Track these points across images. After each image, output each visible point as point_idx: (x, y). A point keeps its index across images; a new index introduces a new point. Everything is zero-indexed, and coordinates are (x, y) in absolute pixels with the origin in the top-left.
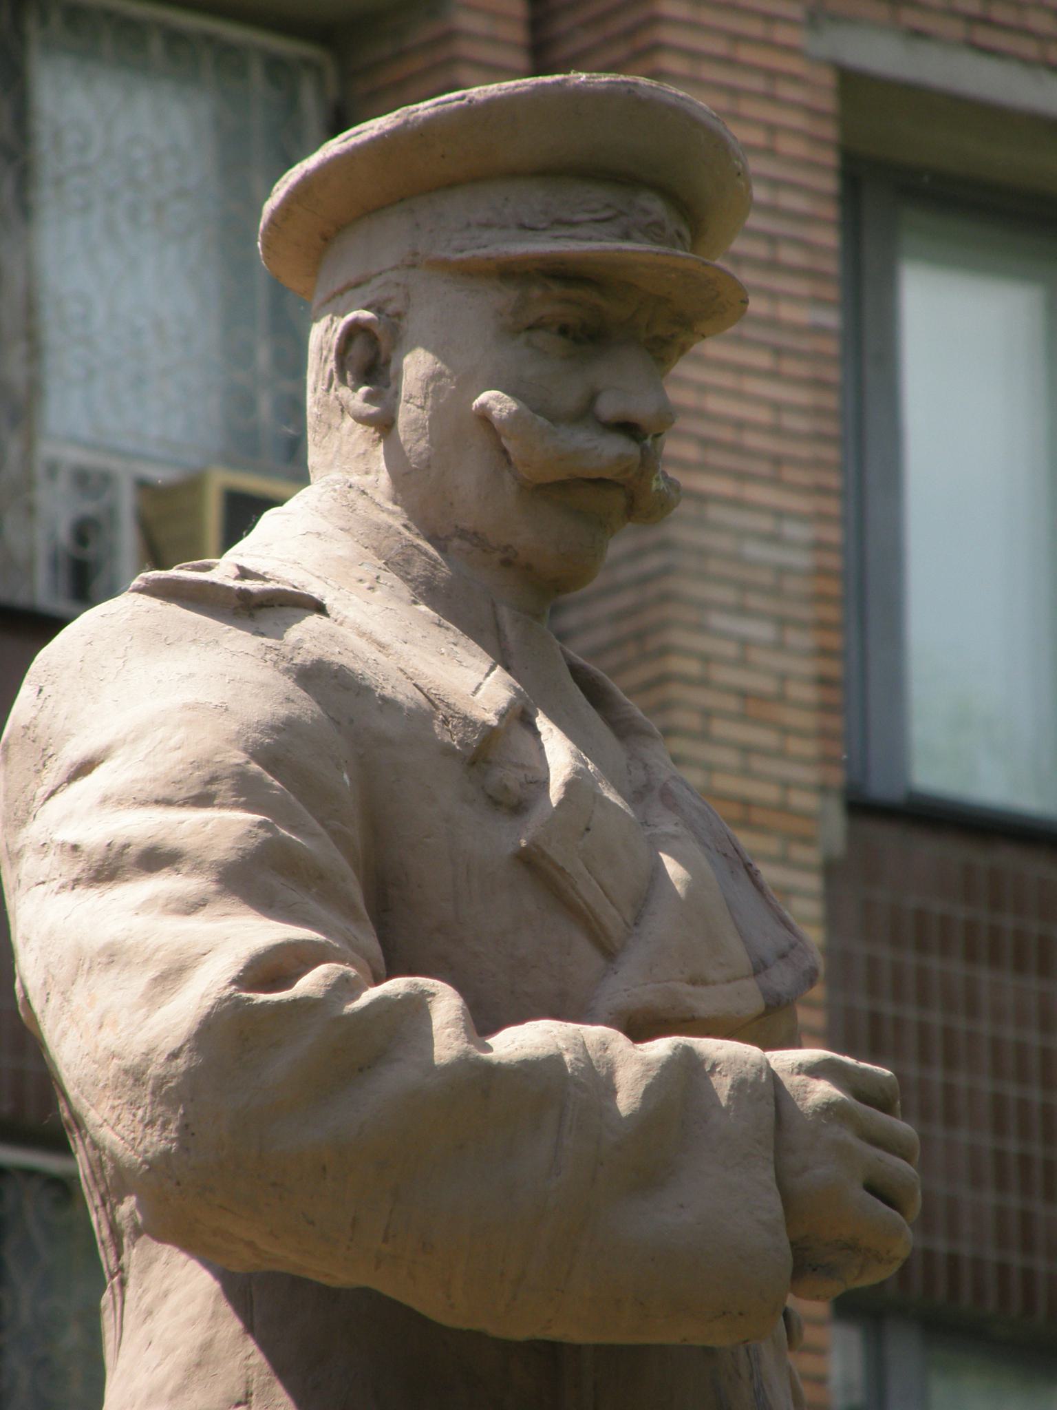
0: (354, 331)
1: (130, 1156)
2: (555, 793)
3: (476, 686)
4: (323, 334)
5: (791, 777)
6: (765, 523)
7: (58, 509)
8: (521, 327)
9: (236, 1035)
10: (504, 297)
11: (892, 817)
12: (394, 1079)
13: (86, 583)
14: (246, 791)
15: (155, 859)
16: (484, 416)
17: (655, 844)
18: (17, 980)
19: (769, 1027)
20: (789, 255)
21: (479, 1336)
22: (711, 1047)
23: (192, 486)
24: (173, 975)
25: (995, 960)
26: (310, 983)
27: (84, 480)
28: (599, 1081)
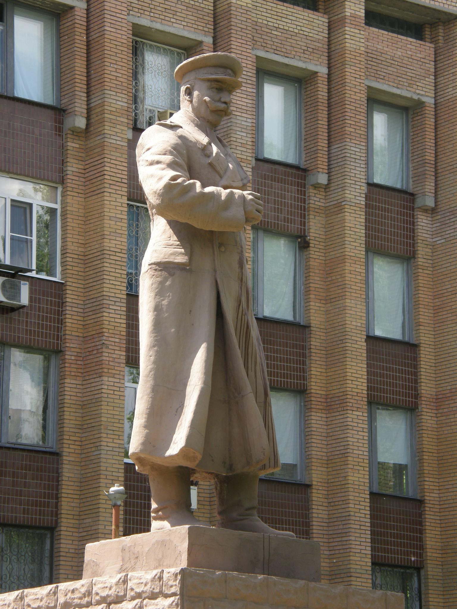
0: (187, 88)
1: (154, 204)
2: (214, 155)
3: (203, 139)
4: (183, 89)
5: (248, 155)
6: (245, 119)
7: (147, 115)
8: (211, 88)
9: (169, 188)
10: (209, 84)
11: (262, 161)
12: (191, 194)
13: (150, 124)
14: (171, 153)
15: (158, 162)
16: (205, 101)
17: (228, 162)
18: (171, 259)
19: (243, 188)
20: (249, 82)
21: (202, 230)
22: (235, 191)
23: (166, 112)
24: (160, 179)
25: (275, 181)
26: (180, 180)
27: (150, 111)
28: (219, 195)
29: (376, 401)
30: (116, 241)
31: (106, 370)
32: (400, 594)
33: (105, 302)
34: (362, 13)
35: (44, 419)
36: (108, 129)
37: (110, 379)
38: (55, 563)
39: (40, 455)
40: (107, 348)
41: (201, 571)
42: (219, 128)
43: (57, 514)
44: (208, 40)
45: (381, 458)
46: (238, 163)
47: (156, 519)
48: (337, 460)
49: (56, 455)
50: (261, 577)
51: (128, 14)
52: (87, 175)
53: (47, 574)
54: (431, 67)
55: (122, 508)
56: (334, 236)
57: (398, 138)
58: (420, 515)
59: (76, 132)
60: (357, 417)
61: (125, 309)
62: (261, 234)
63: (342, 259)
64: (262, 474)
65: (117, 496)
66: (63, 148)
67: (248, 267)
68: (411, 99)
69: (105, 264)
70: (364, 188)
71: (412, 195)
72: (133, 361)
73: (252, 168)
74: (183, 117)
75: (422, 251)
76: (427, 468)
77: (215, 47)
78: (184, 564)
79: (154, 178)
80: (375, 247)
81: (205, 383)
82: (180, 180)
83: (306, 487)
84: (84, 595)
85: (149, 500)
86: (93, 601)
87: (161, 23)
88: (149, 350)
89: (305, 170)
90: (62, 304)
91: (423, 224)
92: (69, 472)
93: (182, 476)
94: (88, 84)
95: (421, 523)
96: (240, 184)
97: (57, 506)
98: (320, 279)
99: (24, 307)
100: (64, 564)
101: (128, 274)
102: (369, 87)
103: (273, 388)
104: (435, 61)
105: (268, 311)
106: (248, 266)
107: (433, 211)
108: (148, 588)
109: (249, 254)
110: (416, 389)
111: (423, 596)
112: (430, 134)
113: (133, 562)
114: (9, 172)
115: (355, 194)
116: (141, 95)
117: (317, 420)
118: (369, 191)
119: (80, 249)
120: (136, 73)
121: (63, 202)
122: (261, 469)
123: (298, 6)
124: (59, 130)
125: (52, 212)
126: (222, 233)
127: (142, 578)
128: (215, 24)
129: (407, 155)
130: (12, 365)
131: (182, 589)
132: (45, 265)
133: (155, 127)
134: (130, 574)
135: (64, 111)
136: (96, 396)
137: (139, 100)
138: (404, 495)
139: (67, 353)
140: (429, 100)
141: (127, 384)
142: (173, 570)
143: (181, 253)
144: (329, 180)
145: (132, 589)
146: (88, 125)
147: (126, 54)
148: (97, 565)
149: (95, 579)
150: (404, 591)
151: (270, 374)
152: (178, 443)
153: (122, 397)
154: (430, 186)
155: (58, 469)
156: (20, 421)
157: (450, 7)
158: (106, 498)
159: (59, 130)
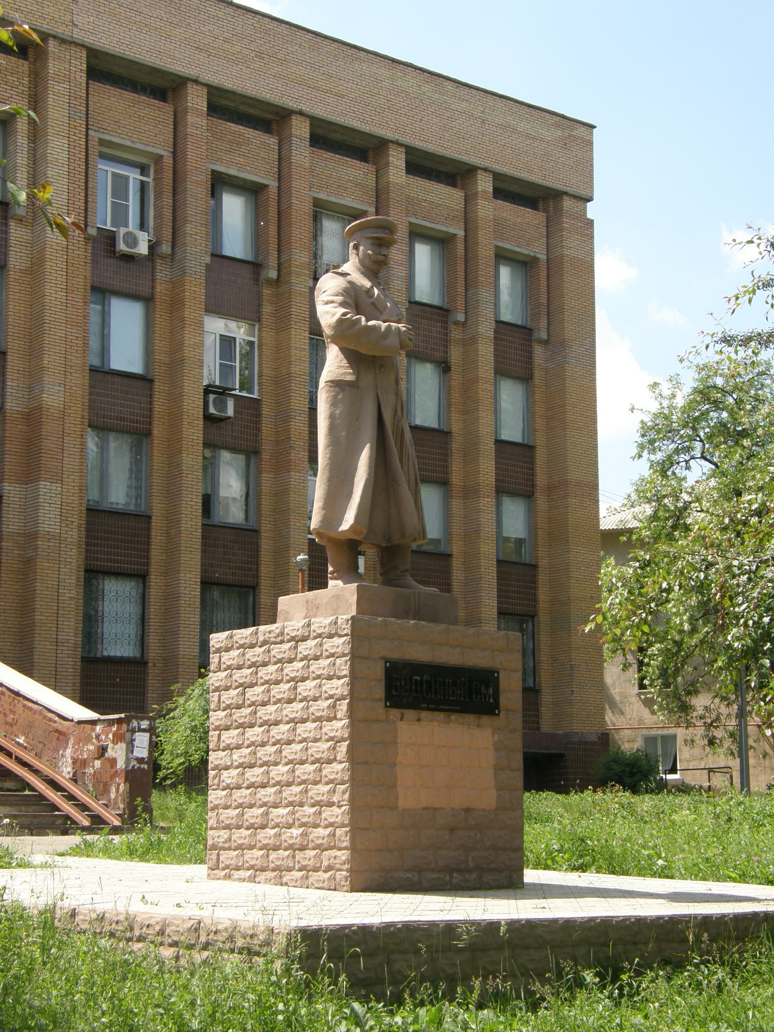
3: (367, 284)
4: (351, 245)
5: (402, 298)
8: (373, 244)
9: (340, 322)
10: (370, 241)
11: (413, 303)
12: (357, 327)
13: (327, 271)
14: (342, 295)
15: (332, 302)
19: (398, 322)
24: (334, 315)
26: (348, 316)
28: (380, 327)
29: (502, 490)
30: (300, 367)
32: (519, 634)
34: (491, 189)
35: (247, 505)
36: (294, 279)
41: (366, 617)
43: (257, 576)
44: (372, 210)
45: (505, 534)
46: (396, 304)
47: (331, 579)
48: (472, 535)
49: (256, 532)
50: (412, 622)
53: (251, 621)
55: (306, 572)
56: (470, 362)
57: (519, 286)
59: (269, 282)
60: (487, 503)
62: (413, 360)
63: (476, 380)
64: (414, 546)
66: (259, 295)
68: (529, 256)
70: (493, 324)
71: (530, 330)
72: (313, 459)
74: (351, 267)
75: (538, 374)
77: (377, 213)
78: (354, 613)
79: (328, 314)
80: (502, 371)
81: (369, 474)
82: (348, 316)
83: (448, 556)
84: (278, 635)
89: (447, 311)
90: (259, 415)
91: (539, 352)
92: (266, 545)
93: (351, 546)
94: (279, 245)
95: (535, 582)
96: (396, 319)
97: (257, 570)
98: (459, 395)
100: (263, 613)
102: (496, 246)
105: (418, 422)
107: (546, 342)
109: (403, 376)
110: (533, 481)
113: (315, 610)
114: (218, 313)
115: (486, 329)
116: (319, 252)
117: (457, 505)
120: (316, 234)
124: (256, 280)
125: (251, 343)
126: (381, 357)
127: (322, 622)
128: (377, 197)
131: (352, 631)
132: (246, 385)
133: (329, 274)
135: (260, 265)
138: (523, 561)
140: (543, 257)
142: (345, 617)
143: (350, 373)
146: (279, 276)
147: (308, 222)
148: (287, 613)
151: (420, 469)
152: (348, 520)
153: (305, 488)
154: (543, 323)
159: (256, 280)
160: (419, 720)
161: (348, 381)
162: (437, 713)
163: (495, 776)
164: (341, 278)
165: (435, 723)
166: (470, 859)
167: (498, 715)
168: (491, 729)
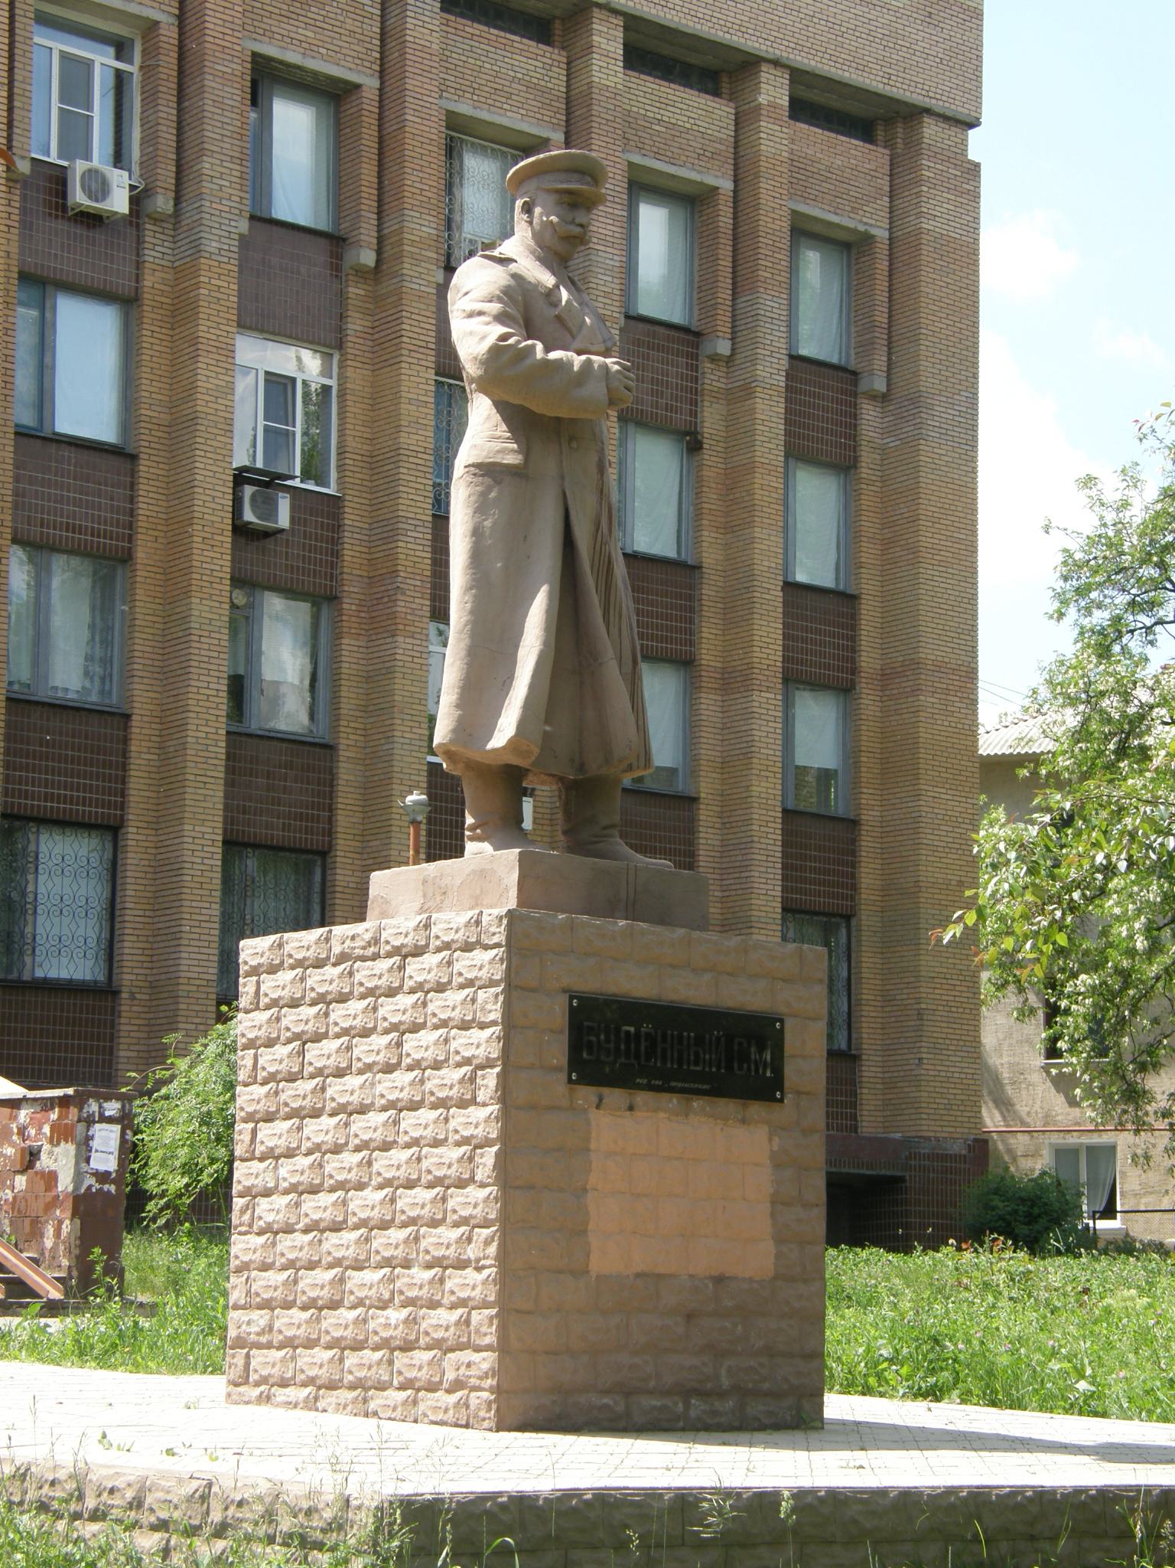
3: (548, 279)
4: (519, 203)
5: (613, 310)
8: (560, 203)
9: (497, 352)
10: (554, 197)
11: (634, 319)
12: (528, 362)
13: (471, 254)
14: (500, 300)
15: (480, 313)
19: (606, 354)
22: (593, 357)
24: (483, 338)
26: (511, 341)
27: (471, 241)
28: (570, 364)
29: (796, 677)
30: (417, 436)
31: (401, 627)
33: (401, 525)
34: (785, 101)
36: (407, 269)
37: (407, 640)
38: (329, 902)
39: (307, 748)
40: (404, 594)
42: (571, 263)
43: (330, 833)
44: (558, 137)
45: (801, 760)
46: (601, 319)
47: (471, 839)
48: (736, 762)
50: (622, 923)
51: (441, 97)
52: (376, 336)
53: (316, 916)
54: (885, 184)
55: (423, 827)
56: (740, 433)
57: (836, 288)
58: (854, 841)
59: (361, 272)
60: (766, 701)
61: (429, 537)
62: (631, 428)
63: (750, 468)
64: (627, 781)
65: (417, 808)
67: (612, 473)
68: (855, 231)
69: (402, 470)
70: (785, 362)
71: (854, 373)
72: (440, 614)
73: (621, 330)
74: (518, 246)
75: (867, 458)
76: (865, 775)
77: (568, 144)
78: (512, 904)
79: (474, 336)
81: (546, 643)
82: (511, 341)
84: (369, 944)
85: (463, 816)
86: (382, 952)
87: (489, 111)
88: (464, 594)
89: (698, 334)
90: (337, 527)
91: (869, 415)
92: (347, 774)
93: (509, 779)
95: (853, 853)
96: (602, 348)
98: (719, 498)
99: (283, 530)
100: (340, 902)
101: (435, 485)
102: (794, 212)
103: (646, 658)
104: (891, 175)
106: (611, 470)
107: (884, 398)
108: (460, 936)
109: (612, 456)
110: (853, 661)
111: (853, 955)
112: (882, 284)
113: (438, 898)
114: (262, 331)
115: (771, 371)
116: (457, 217)
117: (709, 703)
118: (791, 367)
119: (365, 447)
120: (451, 184)
121: (342, 378)
122: (625, 771)
123: (691, 88)
124: (336, 268)
127: (451, 921)
129: (848, 315)
130: (266, 619)
131: (509, 938)
134: (434, 916)
135: (344, 240)
136: (387, 665)
137: (454, 226)
138: (832, 813)
139: (346, 600)
140: (881, 233)
141: (431, 648)
142: (496, 912)
143: (513, 451)
144: (733, 349)
145: (437, 937)
146: (379, 261)
149: (384, 922)
150: (827, 944)
151: (641, 636)
153: (425, 667)
154: (880, 361)
155: (331, 768)
156: (276, 702)
157: (914, 96)
158: (401, 811)
159: (336, 268)
160: (631, 1108)
161: (507, 466)
162: (665, 1097)
163: (773, 1215)
164: (499, 268)
165: (662, 1115)
166: (723, 1372)
167: (781, 1100)
168: (766, 1128)
